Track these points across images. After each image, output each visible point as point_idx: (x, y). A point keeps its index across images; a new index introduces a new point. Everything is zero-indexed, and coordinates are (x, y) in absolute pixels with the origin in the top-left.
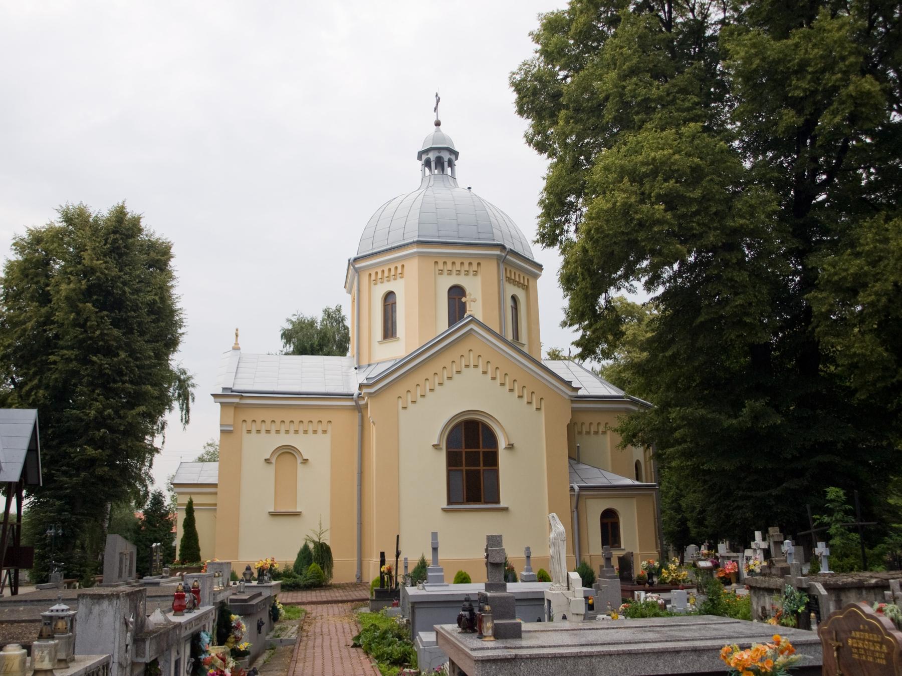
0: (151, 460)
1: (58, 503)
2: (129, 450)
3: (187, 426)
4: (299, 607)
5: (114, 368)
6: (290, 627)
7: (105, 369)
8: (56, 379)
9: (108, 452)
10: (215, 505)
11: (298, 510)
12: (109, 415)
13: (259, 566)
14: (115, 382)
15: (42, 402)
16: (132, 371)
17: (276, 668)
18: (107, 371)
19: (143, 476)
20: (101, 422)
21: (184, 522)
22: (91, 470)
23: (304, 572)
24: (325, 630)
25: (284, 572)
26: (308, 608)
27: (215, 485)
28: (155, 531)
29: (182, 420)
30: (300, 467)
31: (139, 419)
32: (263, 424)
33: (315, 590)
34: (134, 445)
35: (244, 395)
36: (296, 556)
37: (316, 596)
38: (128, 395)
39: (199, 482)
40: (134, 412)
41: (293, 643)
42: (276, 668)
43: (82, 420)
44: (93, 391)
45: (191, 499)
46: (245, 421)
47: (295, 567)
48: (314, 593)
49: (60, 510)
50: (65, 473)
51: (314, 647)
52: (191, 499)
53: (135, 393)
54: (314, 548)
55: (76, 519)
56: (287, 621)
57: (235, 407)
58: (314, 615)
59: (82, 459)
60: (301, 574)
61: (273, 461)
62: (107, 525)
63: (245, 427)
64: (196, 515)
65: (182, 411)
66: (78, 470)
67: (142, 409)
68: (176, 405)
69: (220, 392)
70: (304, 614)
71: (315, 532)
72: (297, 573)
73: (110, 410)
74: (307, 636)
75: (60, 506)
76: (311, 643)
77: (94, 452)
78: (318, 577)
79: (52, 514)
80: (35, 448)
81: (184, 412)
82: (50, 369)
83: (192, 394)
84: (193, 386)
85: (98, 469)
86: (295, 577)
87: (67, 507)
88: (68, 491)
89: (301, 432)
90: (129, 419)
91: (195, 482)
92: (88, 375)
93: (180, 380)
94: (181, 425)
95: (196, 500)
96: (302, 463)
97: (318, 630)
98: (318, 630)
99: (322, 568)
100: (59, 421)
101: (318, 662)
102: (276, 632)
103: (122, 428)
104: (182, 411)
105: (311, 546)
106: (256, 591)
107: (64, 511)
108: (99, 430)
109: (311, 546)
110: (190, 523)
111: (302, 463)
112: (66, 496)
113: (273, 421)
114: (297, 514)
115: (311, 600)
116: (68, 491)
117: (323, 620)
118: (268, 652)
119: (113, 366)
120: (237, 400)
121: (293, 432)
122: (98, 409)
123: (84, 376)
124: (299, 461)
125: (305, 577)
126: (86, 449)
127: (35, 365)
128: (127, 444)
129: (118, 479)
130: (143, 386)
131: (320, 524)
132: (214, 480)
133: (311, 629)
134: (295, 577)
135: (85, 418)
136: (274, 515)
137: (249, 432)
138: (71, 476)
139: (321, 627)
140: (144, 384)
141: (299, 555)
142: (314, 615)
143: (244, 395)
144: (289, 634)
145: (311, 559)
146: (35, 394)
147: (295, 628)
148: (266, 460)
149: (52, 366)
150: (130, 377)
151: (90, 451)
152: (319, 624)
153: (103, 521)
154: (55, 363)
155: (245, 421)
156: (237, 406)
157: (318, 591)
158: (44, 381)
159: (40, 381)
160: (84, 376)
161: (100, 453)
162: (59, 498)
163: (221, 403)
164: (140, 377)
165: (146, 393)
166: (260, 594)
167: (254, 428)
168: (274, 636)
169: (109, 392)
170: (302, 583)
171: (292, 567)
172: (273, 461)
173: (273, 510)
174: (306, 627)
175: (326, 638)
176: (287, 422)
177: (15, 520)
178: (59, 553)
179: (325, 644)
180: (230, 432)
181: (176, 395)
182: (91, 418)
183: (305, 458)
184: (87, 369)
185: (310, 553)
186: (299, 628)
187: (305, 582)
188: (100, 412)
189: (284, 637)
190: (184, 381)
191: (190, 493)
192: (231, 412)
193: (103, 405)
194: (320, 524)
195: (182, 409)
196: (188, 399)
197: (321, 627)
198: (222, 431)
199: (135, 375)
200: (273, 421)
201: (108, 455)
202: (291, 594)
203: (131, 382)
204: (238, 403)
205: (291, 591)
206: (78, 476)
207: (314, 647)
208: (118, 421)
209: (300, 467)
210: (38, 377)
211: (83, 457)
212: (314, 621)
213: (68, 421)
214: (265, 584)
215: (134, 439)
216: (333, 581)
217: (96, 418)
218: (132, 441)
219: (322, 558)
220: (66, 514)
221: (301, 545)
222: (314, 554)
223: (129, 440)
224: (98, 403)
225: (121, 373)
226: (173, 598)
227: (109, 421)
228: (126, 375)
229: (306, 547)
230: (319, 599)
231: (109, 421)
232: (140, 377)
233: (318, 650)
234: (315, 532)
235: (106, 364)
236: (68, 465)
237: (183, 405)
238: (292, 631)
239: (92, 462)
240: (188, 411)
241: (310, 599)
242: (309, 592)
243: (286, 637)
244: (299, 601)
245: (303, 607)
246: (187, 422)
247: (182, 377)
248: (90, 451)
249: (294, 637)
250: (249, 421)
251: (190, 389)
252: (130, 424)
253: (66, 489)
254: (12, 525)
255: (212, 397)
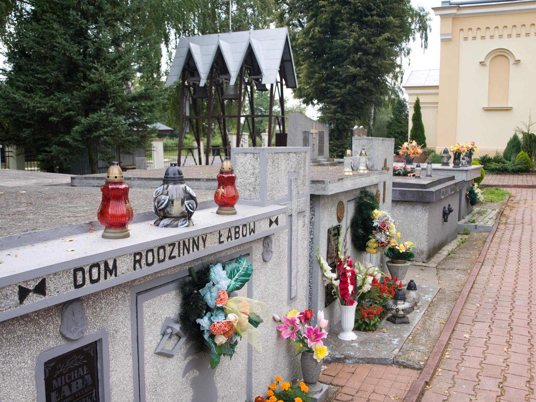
0: (402, 78)
1: (333, 107)
2: (379, 67)
3: (426, 50)
4: (505, 189)
5: (365, 6)
6: (489, 210)
7: (358, 7)
8: (326, 18)
9: (364, 69)
10: (437, 103)
11: (509, 106)
12: (363, 42)
13: (455, 149)
14: (366, 16)
15: (317, 36)
16: (378, 7)
17: (458, 266)
18: (360, 8)
19: (397, 89)
20: (357, 47)
21: (413, 117)
22: (354, 84)
23: (512, 158)
24: (527, 218)
25: (494, 158)
26: (513, 191)
27: (436, 87)
28: (401, 127)
29: (422, 46)
30: (512, 68)
31: (387, 43)
32: (479, 31)
33: (522, 175)
34: (382, 63)
35: (460, 6)
36: (506, 145)
37: (522, 180)
38: (377, 25)
39: (426, 85)
40: (381, 38)
41: (488, 230)
42: (458, 266)
43: (345, 47)
44: (351, 25)
45: (418, 98)
46: (462, 30)
47: (505, 154)
48: (520, 177)
49: (335, 112)
50: (337, 86)
51: (510, 241)
52: (418, 98)
53: (382, 23)
54: (523, 138)
55: (345, 117)
56: (489, 204)
57: (453, 18)
58: (517, 198)
59: (347, 75)
60: (510, 160)
61: (488, 63)
62: (372, 123)
63: (462, 35)
64: (422, 111)
65: (422, 39)
66: (346, 83)
67: (387, 35)
68: (418, 35)
69: (440, 5)
70: (507, 197)
71: (524, 124)
72: (506, 159)
73: (364, 38)
74: (506, 223)
75: (334, 109)
76: (508, 234)
77: (354, 70)
78: (525, 163)
79: (330, 115)
80: (289, 59)
81: (424, 40)
82: (322, 12)
83: (430, 26)
84: (430, 20)
85: (358, 83)
86: (504, 163)
87: (339, 109)
88: (339, 99)
89: (514, 35)
90: (378, 43)
91: (422, 85)
92: (347, 13)
93: (420, 16)
94: (422, 50)
95: (422, 100)
96: (514, 64)
97: (519, 217)
98: (519, 217)
99: (530, 156)
100: (331, 49)
101: (512, 267)
102: (473, 216)
103: (373, 51)
104: (422, 39)
105: (520, 136)
106: (451, 174)
107: (337, 112)
108: (357, 54)
109: (520, 136)
110: (417, 117)
111: (514, 64)
112: (338, 102)
113: (488, 28)
114: (508, 109)
115: (516, 184)
116: (339, 99)
117: (526, 205)
118: (459, 237)
119: (364, 4)
120: (454, 11)
121: (506, 36)
122: (355, 38)
123: (344, 14)
124: (512, 62)
125: (513, 163)
126: (349, 68)
127: (312, 10)
128: (377, 63)
129: (373, 89)
130: (387, 18)
131: (530, 117)
132: (435, 82)
133: (512, 215)
134: (504, 163)
135: (347, 45)
136: (487, 110)
137: (466, 39)
138: (341, 88)
139: (523, 214)
140: (388, 16)
141: (508, 144)
142: (517, 198)
143: (460, 6)
144: (487, 219)
145: (520, 148)
146: (313, 31)
147: (495, 212)
148: (480, 63)
149: (323, 9)
150: (377, 11)
151: (352, 70)
152: (521, 210)
153: (369, 120)
154: (324, 6)
155: (462, 30)
156: (455, 17)
157: (524, 176)
158: (318, 21)
159: (316, 21)
160: (344, 14)
161: (358, 70)
162: (334, 104)
163: (441, 15)
164: (385, 11)
165: (390, 23)
166: (453, 178)
167: (470, 35)
168: (470, 221)
169: (362, 24)
170: (510, 168)
171: (502, 154)
172: (488, 63)
173: (487, 106)
174: (506, 212)
175: (527, 228)
176: (501, 27)
177: (280, 114)
178: (336, 141)
179: (524, 238)
180: (449, 40)
181: (418, 27)
182: (351, 45)
183: (517, 59)
184: (345, 8)
185: (519, 143)
186: (498, 213)
187: (513, 168)
188: (357, 40)
189: (480, 223)
190: (423, 16)
191: (417, 94)
192: (450, 22)
193: (358, 35)
194: (530, 117)
195: (421, 37)
196: (426, 30)
197: (523, 214)
198: (442, 40)
199: (381, 10)
200: (488, 28)
201: (364, 72)
202: (499, 177)
203: (378, 15)
204: (455, 15)
205: (500, 174)
206: (345, 87)
207: (510, 241)
208: (370, 45)
209: (512, 68)
210: (314, 19)
211: (348, 74)
212: (516, 205)
213: (337, 48)
214: (461, 168)
215: (383, 59)
216: (353, 201)
217: (354, 44)
218: (381, 60)
219: (530, 148)
220: (339, 115)
221: (510, 136)
222: (522, 143)
223: (379, 60)
224: (354, 33)
225: (370, 9)
226: (216, 184)
227: (363, 46)
228: (373, 10)
229: (515, 138)
230: (525, 183)
231: (363, 46)
232: (385, 11)
233: (514, 246)
234: (524, 124)
235: (359, 3)
236: (339, 81)
237: (422, 35)
238: (490, 216)
239: (354, 77)
240: (426, 39)
241: (515, 183)
242: (516, 176)
243: (482, 224)
244: (505, 184)
245: (508, 190)
246: (426, 47)
247: (421, 14)
248: (352, 70)
249: (490, 223)
250: (466, 29)
251: (428, 23)
252: (379, 47)
253: (338, 97)
254: (277, 118)
255: (433, 11)
